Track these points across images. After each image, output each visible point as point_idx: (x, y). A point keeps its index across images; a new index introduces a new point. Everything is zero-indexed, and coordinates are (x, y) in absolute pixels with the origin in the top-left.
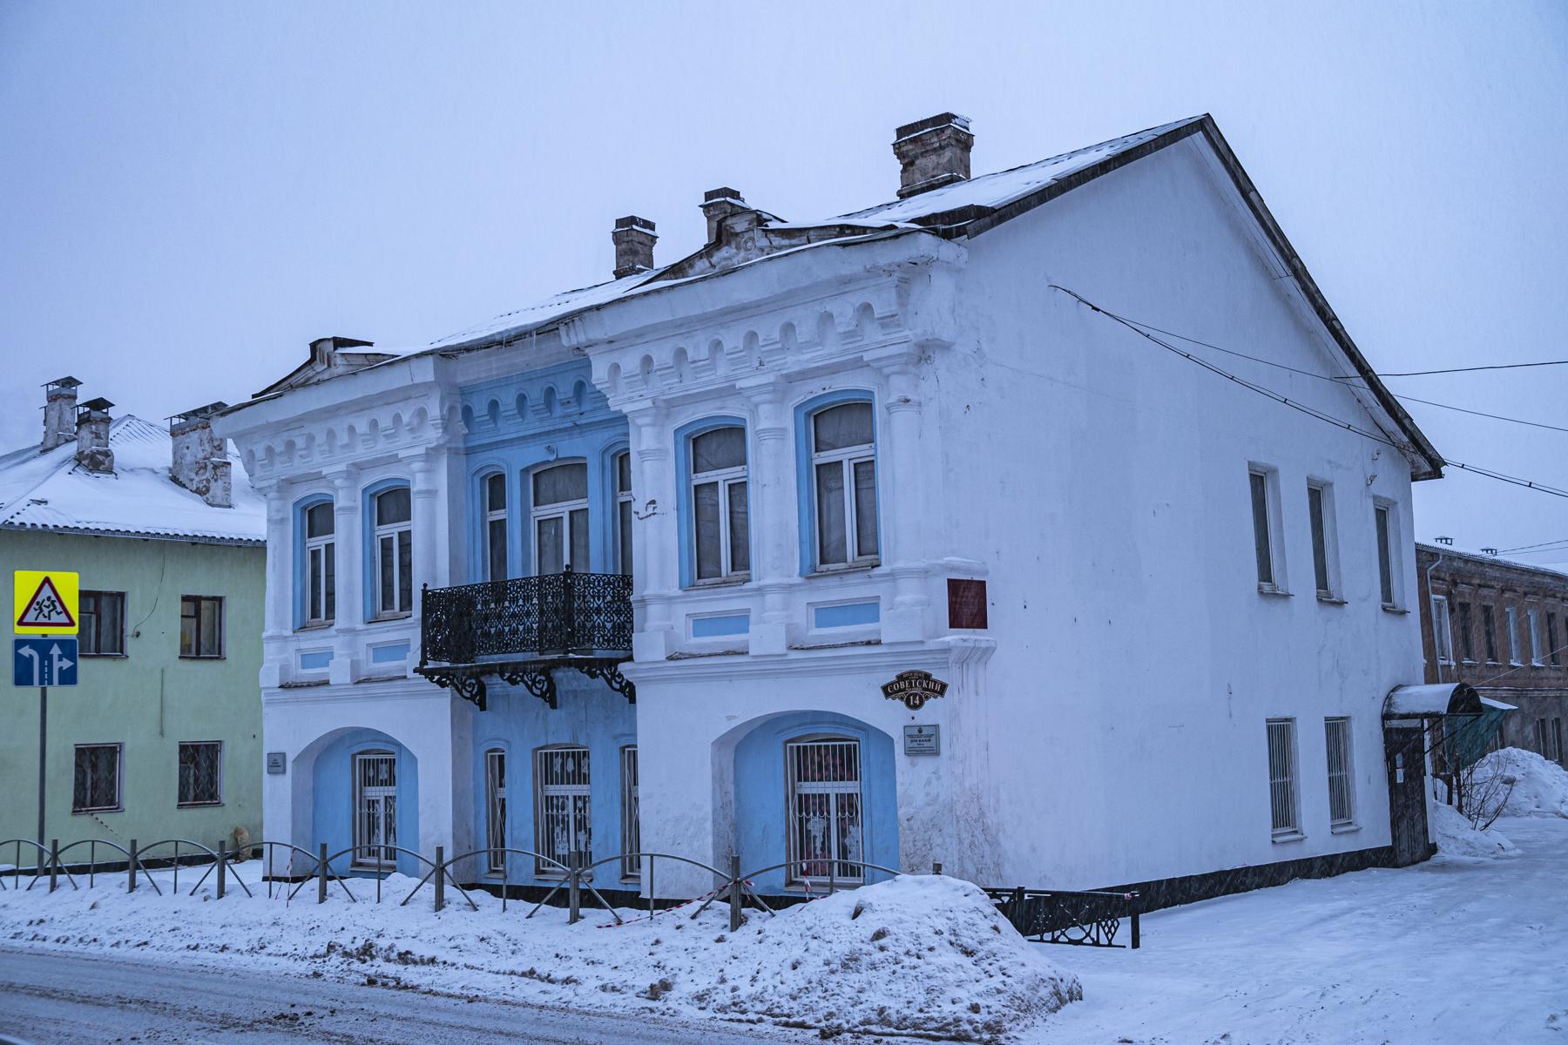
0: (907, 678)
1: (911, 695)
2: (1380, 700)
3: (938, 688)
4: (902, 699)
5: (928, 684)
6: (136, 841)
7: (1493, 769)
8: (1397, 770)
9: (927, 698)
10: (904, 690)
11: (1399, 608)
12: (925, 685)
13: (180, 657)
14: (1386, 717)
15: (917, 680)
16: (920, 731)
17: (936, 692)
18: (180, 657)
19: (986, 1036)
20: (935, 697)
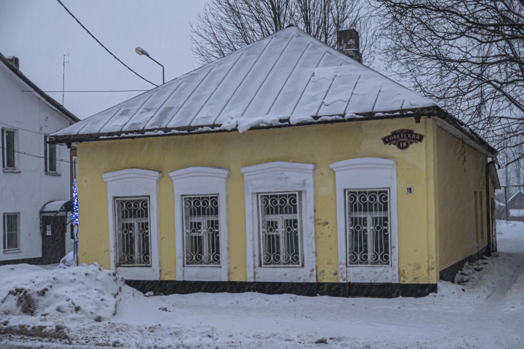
0: (398, 133)
1: (401, 142)
2: (42, 205)
3: (418, 137)
4: (395, 144)
5: (411, 136)
8: (47, 231)
9: (411, 143)
11: (59, 174)
12: (409, 136)
14: (41, 212)
15: (404, 134)
17: (417, 140)
20: (416, 142)
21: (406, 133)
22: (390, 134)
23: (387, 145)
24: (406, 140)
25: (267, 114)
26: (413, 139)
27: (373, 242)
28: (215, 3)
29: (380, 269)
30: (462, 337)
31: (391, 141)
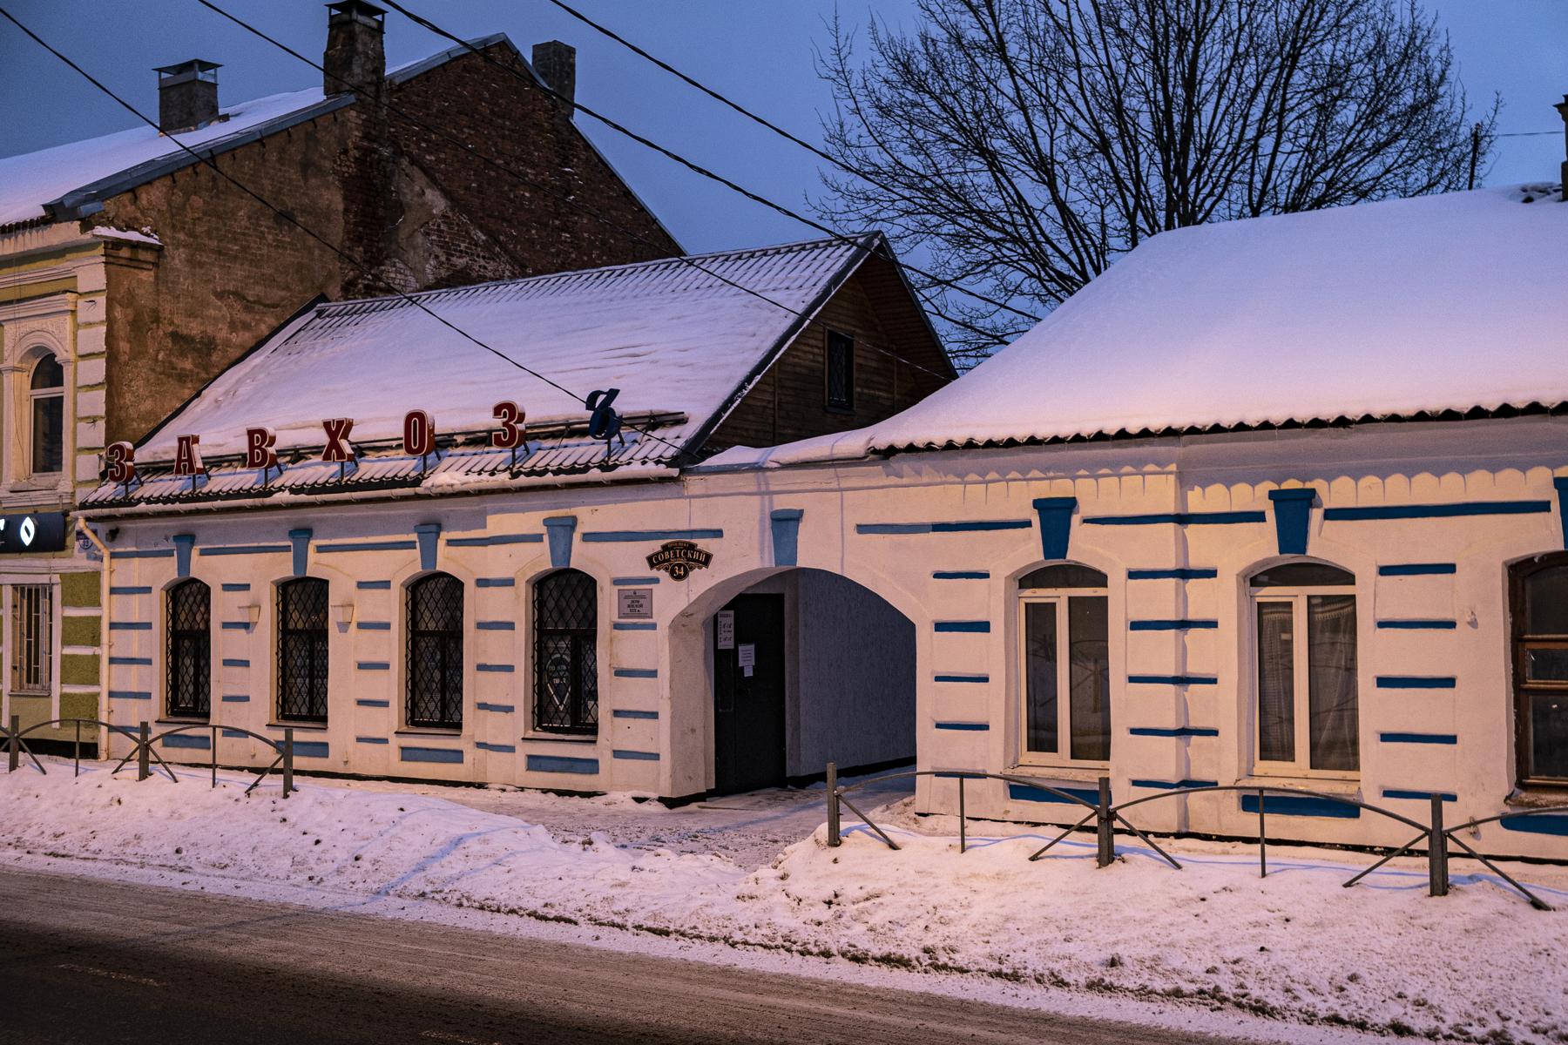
0: (672, 548)
1: (677, 565)
3: (703, 558)
4: (666, 569)
5: (692, 555)
9: (691, 569)
17: (701, 562)
20: (700, 568)
28: (85, 859)
29: (1072, 595)
31: (660, 563)
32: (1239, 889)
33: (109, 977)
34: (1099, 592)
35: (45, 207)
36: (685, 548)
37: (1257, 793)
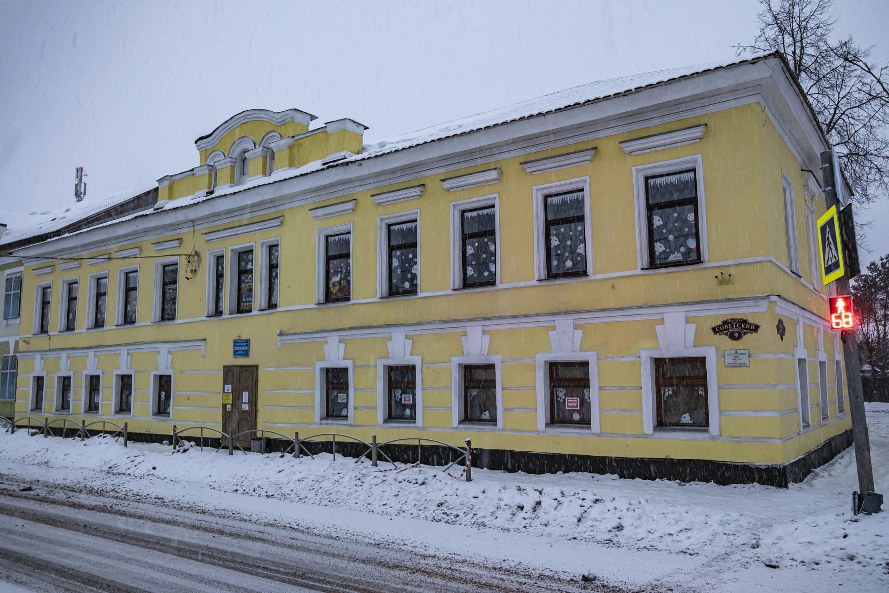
0: (730, 323)
3: (753, 327)
4: (727, 334)
5: (745, 326)
6: (129, 377)
7: (882, 299)
9: (744, 333)
10: (728, 329)
13: (177, 264)
16: (736, 352)
17: (752, 330)
18: (177, 264)
19: (396, 591)
21: (739, 322)
22: (720, 323)
23: (717, 335)
24: (738, 330)
25: (30, 214)
26: (747, 329)
27: (485, 424)
30: (663, 514)
31: (721, 331)
32: (233, 491)
33: (547, 465)
34: (267, 174)
35: (786, 487)
36: (739, 322)
37: (416, 443)
